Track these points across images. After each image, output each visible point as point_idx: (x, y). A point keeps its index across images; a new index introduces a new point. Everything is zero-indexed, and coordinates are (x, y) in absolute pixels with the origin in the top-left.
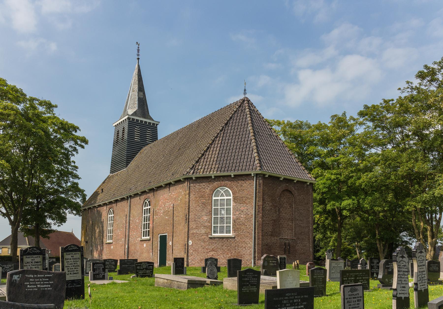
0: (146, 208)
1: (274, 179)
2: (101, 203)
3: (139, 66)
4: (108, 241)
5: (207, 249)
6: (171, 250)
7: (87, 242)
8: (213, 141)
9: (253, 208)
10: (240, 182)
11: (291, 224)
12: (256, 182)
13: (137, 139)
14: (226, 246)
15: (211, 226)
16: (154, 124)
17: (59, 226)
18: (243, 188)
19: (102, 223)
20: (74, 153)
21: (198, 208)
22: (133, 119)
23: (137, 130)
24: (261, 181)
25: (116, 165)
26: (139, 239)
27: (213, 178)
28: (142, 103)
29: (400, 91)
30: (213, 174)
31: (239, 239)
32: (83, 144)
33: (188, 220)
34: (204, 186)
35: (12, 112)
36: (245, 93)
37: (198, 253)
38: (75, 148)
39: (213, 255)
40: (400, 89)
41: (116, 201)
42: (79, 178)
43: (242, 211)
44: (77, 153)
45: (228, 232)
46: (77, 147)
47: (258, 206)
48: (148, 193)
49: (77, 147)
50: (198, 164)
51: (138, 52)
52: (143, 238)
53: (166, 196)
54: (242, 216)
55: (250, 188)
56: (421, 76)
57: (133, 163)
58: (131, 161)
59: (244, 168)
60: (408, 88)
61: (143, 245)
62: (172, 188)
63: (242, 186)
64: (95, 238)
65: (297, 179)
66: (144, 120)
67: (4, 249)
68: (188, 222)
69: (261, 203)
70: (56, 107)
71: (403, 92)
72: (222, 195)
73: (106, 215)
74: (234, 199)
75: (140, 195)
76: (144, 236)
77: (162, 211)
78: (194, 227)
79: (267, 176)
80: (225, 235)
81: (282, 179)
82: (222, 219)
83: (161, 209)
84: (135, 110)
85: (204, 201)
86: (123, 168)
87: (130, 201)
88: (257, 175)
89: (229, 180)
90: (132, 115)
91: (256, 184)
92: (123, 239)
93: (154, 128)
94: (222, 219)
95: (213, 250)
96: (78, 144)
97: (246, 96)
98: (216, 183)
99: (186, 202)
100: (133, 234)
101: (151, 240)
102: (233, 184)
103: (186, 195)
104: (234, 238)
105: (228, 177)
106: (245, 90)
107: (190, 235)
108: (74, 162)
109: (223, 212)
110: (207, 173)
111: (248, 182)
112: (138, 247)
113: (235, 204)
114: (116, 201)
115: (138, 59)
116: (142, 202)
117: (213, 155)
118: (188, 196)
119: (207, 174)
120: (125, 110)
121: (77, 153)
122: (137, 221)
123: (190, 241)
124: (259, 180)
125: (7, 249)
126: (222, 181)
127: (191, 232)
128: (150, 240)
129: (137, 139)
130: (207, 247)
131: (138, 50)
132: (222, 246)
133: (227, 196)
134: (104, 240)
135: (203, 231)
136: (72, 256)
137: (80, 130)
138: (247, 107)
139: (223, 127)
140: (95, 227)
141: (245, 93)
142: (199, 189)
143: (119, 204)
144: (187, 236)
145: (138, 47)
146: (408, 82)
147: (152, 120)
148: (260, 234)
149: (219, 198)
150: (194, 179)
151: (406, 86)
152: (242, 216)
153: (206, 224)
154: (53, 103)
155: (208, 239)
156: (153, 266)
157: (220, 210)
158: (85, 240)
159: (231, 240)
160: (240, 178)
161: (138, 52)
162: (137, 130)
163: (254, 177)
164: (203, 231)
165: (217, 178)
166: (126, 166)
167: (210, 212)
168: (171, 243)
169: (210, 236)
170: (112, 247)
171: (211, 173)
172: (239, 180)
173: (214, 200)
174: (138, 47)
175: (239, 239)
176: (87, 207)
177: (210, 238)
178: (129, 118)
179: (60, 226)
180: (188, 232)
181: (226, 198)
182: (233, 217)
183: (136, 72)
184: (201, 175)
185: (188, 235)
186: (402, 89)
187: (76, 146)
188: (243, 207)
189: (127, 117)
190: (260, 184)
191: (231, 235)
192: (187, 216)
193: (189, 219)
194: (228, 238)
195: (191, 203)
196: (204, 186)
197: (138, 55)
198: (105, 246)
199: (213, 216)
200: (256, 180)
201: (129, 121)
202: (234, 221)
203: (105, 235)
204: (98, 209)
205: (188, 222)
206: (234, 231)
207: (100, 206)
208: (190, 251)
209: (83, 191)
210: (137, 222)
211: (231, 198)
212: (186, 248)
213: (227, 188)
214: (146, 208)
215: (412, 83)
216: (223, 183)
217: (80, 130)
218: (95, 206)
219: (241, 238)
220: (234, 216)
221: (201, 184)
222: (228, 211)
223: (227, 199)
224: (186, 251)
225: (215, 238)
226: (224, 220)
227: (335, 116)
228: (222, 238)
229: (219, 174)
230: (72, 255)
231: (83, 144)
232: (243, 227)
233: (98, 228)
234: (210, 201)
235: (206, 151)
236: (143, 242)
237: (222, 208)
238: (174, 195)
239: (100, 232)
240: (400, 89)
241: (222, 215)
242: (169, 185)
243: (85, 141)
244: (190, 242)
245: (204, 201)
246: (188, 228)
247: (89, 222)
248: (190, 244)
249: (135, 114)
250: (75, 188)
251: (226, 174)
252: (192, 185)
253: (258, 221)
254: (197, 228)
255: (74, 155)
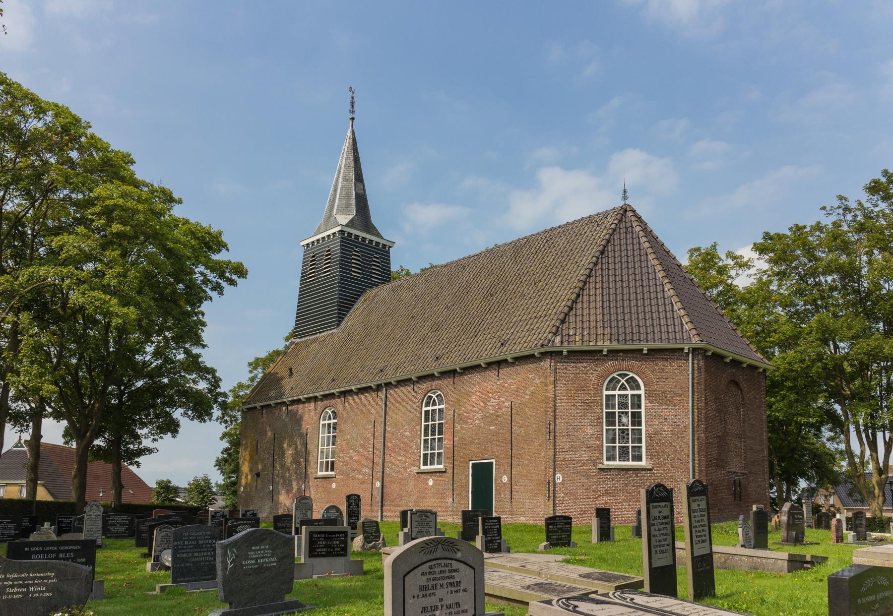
0: (430, 408)
1: (718, 358)
2: (301, 397)
3: (353, 132)
4: (319, 474)
5: (593, 491)
6: (508, 493)
7: (258, 475)
8: (585, 283)
9: (687, 414)
10: (660, 363)
11: (739, 445)
12: (693, 364)
13: (356, 273)
14: (634, 486)
15: (602, 446)
16: (384, 246)
17: (155, 440)
18: (666, 375)
19: (304, 437)
20: (214, 294)
21: (574, 411)
22: (350, 234)
23: (356, 253)
24: (701, 363)
25: (308, 321)
26: (415, 470)
27: (605, 353)
28: (362, 202)
29: (824, 212)
30: (605, 345)
31: (661, 472)
32: (234, 277)
33: (552, 433)
34: (585, 368)
35: (140, 207)
36: (625, 198)
37: (576, 499)
38: (218, 284)
39: (606, 503)
40: (824, 208)
41: (345, 394)
42: (204, 346)
43: (666, 419)
44: (221, 294)
45: (639, 458)
46: (224, 284)
47: (698, 409)
48: (438, 378)
49: (224, 284)
50: (565, 326)
51: (352, 106)
52: (423, 467)
53: (489, 385)
54: (665, 428)
55: (684, 374)
56: (874, 188)
57: (352, 319)
58: (345, 315)
59: (650, 337)
60: (839, 207)
61: (426, 482)
62: (504, 371)
63: (663, 370)
64: (283, 466)
65: (749, 361)
66: (369, 237)
67: (9, 488)
68: (555, 437)
69: (702, 404)
70: (180, 202)
71: (829, 214)
72: (623, 388)
73: (316, 419)
74: (648, 395)
75: (414, 383)
76: (425, 464)
77: (479, 416)
78: (566, 447)
79: (710, 353)
80: (631, 463)
81: (728, 360)
82: (623, 432)
83: (474, 412)
84: (351, 217)
85: (587, 397)
86: (329, 327)
87: (386, 394)
88: (694, 350)
89: (636, 359)
90: (347, 225)
91: (693, 367)
92: (367, 470)
93: (383, 252)
94: (623, 432)
95: (607, 493)
96: (224, 277)
97: (627, 202)
98: (610, 364)
99: (547, 398)
100: (395, 461)
101: (450, 471)
102: (647, 367)
103: (546, 385)
104: (651, 470)
105: (636, 353)
106: (625, 191)
107: (558, 463)
108: (203, 314)
109: (624, 420)
110: (591, 344)
111: (675, 364)
112: (411, 485)
113: (650, 405)
114: (345, 394)
115: (353, 119)
116: (420, 396)
117: (591, 309)
118: (551, 387)
119: (591, 345)
120: (330, 215)
121: (221, 294)
122: (407, 433)
123: (558, 475)
124: (698, 360)
125: (17, 488)
126: (623, 360)
127: (560, 457)
128: (445, 472)
129: (356, 273)
130: (594, 487)
131: (352, 103)
132: (626, 485)
133: (632, 389)
134: (310, 471)
135: (585, 456)
136: (660, 512)
137: (228, 250)
138: (635, 224)
139: (598, 258)
140: (282, 443)
141: (625, 198)
142: (576, 374)
143: (352, 400)
144: (552, 465)
145: (353, 98)
146: (841, 198)
147: (381, 237)
148: (704, 463)
149: (617, 392)
150: (565, 353)
151: (837, 203)
152: (665, 428)
153: (592, 442)
154: (176, 196)
155: (596, 471)
156: (570, 524)
157: (620, 416)
158: (251, 470)
159: (643, 473)
160: (657, 355)
161: (352, 106)
162: (356, 253)
163: (688, 354)
164: (585, 456)
165: (613, 354)
166: (338, 325)
167: (599, 418)
168: (505, 479)
169: (600, 466)
170: (334, 485)
171: (599, 343)
172: (657, 359)
173: (607, 396)
174: (353, 98)
175: (661, 472)
176: (261, 404)
177: (601, 469)
178: (342, 232)
179: (156, 440)
180: (555, 457)
181: (629, 392)
182: (647, 431)
183: (347, 145)
184: (578, 346)
185: (554, 462)
186: (828, 208)
187: (220, 281)
188: (666, 411)
189: (339, 228)
190: (699, 369)
191: (643, 463)
192: (552, 427)
193: (555, 432)
194: (638, 469)
195: (558, 401)
196: (585, 368)
197: (352, 112)
198: (312, 482)
199: (605, 427)
200: (693, 360)
201: (342, 238)
202: (649, 437)
203: (312, 459)
204: (290, 408)
205: (555, 437)
206: (650, 456)
207: (299, 401)
208: (560, 495)
209: (212, 371)
210: (407, 437)
211: (642, 392)
212: (551, 488)
213: (631, 375)
214: (430, 408)
215: (846, 199)
216: (625, 364)
217: (228, 250)
218: (285, 403)
219: (664, 471)
220: (649, 428)
221: (579, 365)
222: (636, 418)
223: (633, 395)
224: (552, 495)
225: (610, 469)
226: (628, 434)
227: (698, 249)
228: (627, 470)
229: (615, 346)
230: (660, 509)
231: (234, 277)
232: (667, 450)
233: (289, 445)
234: (598, 398)
235: (575, 302)
236: (424, 477)
237: (623, 413)
238: (511, 384)
239: (297, 455)
240: (824, 208)
241: (623, 425)
242: (500, 364)
243: (240, 271)
244: (559, 478)
245: (587, 397)
246: (555, 449)
247: (264, 433)
248: (558, 481)
249: (351, 224)
250: (194, 365)
251: (629, 346)
252: (559, 365)
253: (698, 439)
254: (572, 449)
255: (211, 299)
